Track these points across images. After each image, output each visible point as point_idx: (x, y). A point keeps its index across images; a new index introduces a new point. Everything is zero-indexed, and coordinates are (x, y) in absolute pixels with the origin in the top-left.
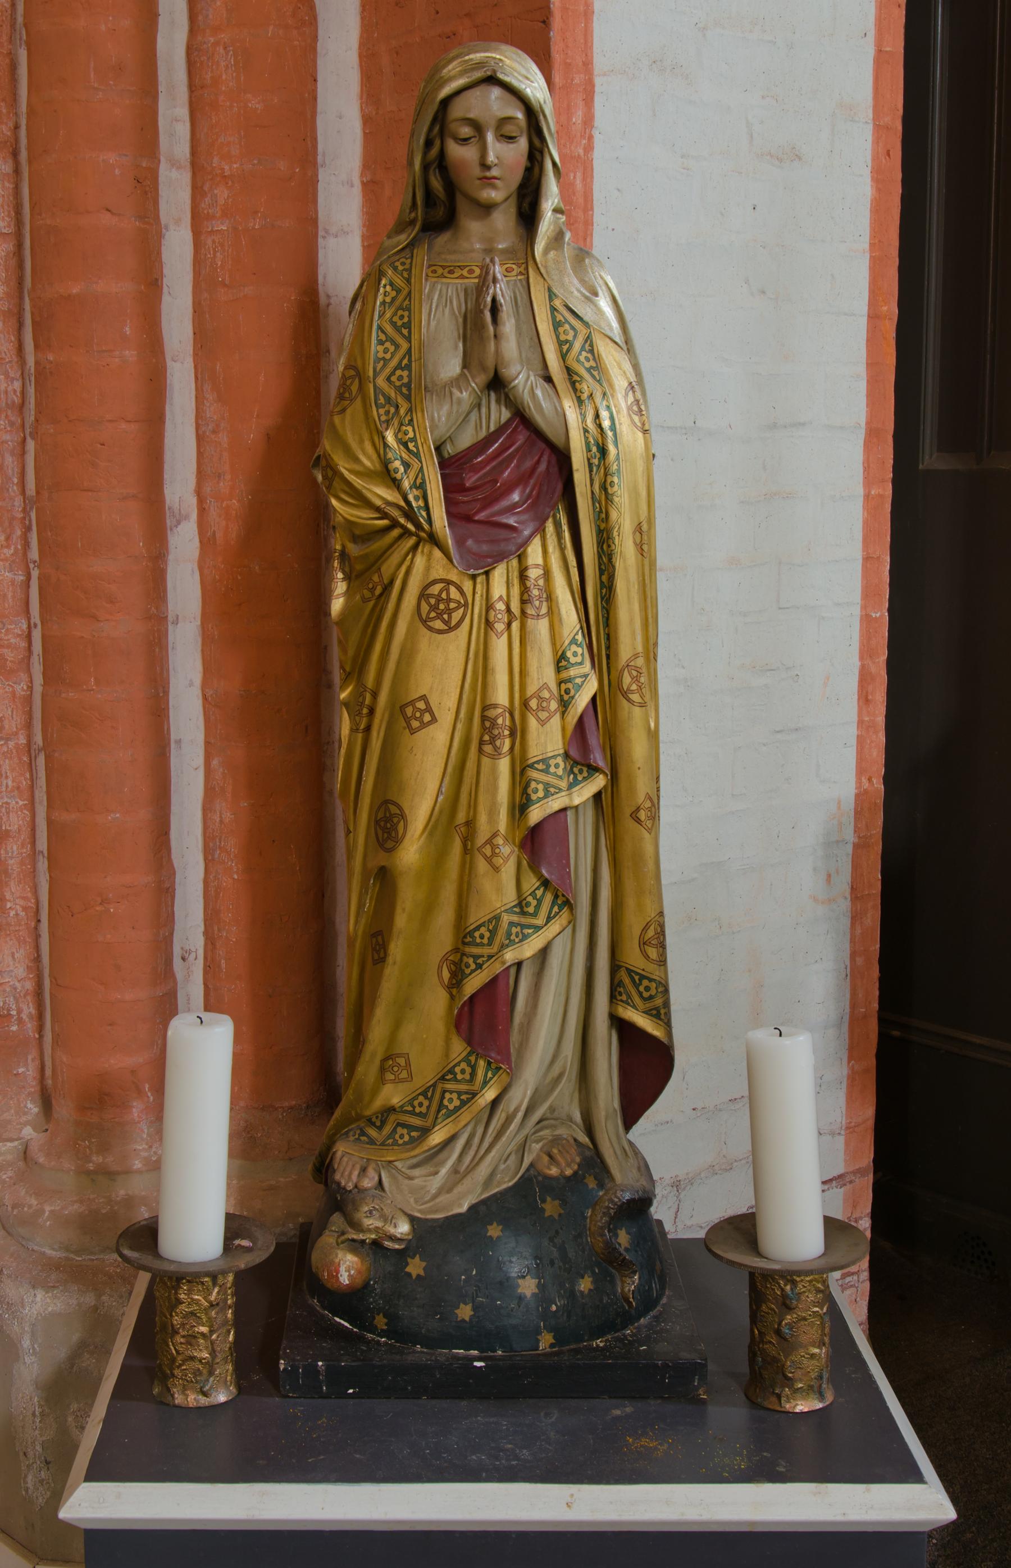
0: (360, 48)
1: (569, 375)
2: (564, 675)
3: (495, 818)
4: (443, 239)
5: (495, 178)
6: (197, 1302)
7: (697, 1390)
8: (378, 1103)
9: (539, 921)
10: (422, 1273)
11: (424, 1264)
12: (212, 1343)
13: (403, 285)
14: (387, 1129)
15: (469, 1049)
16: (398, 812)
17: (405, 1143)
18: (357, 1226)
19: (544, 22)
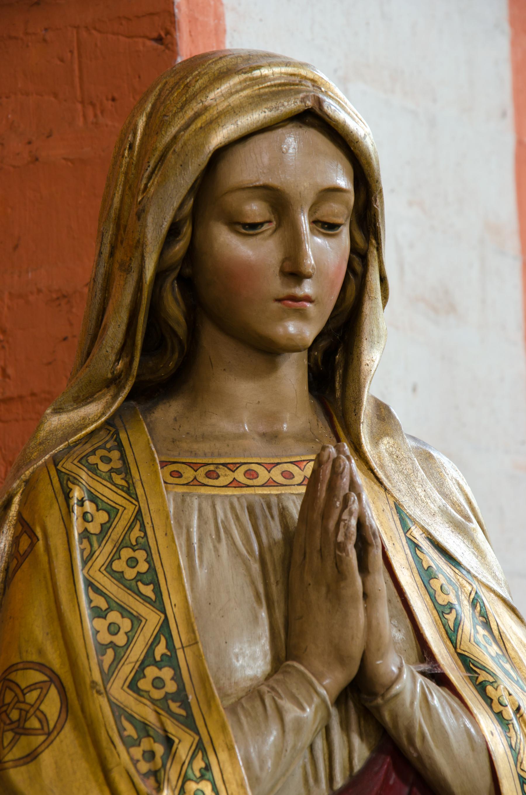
1: (468, 669)
4: (167, 413)
5: (308, 299)
13: (119, 500)
19: (159, 40)
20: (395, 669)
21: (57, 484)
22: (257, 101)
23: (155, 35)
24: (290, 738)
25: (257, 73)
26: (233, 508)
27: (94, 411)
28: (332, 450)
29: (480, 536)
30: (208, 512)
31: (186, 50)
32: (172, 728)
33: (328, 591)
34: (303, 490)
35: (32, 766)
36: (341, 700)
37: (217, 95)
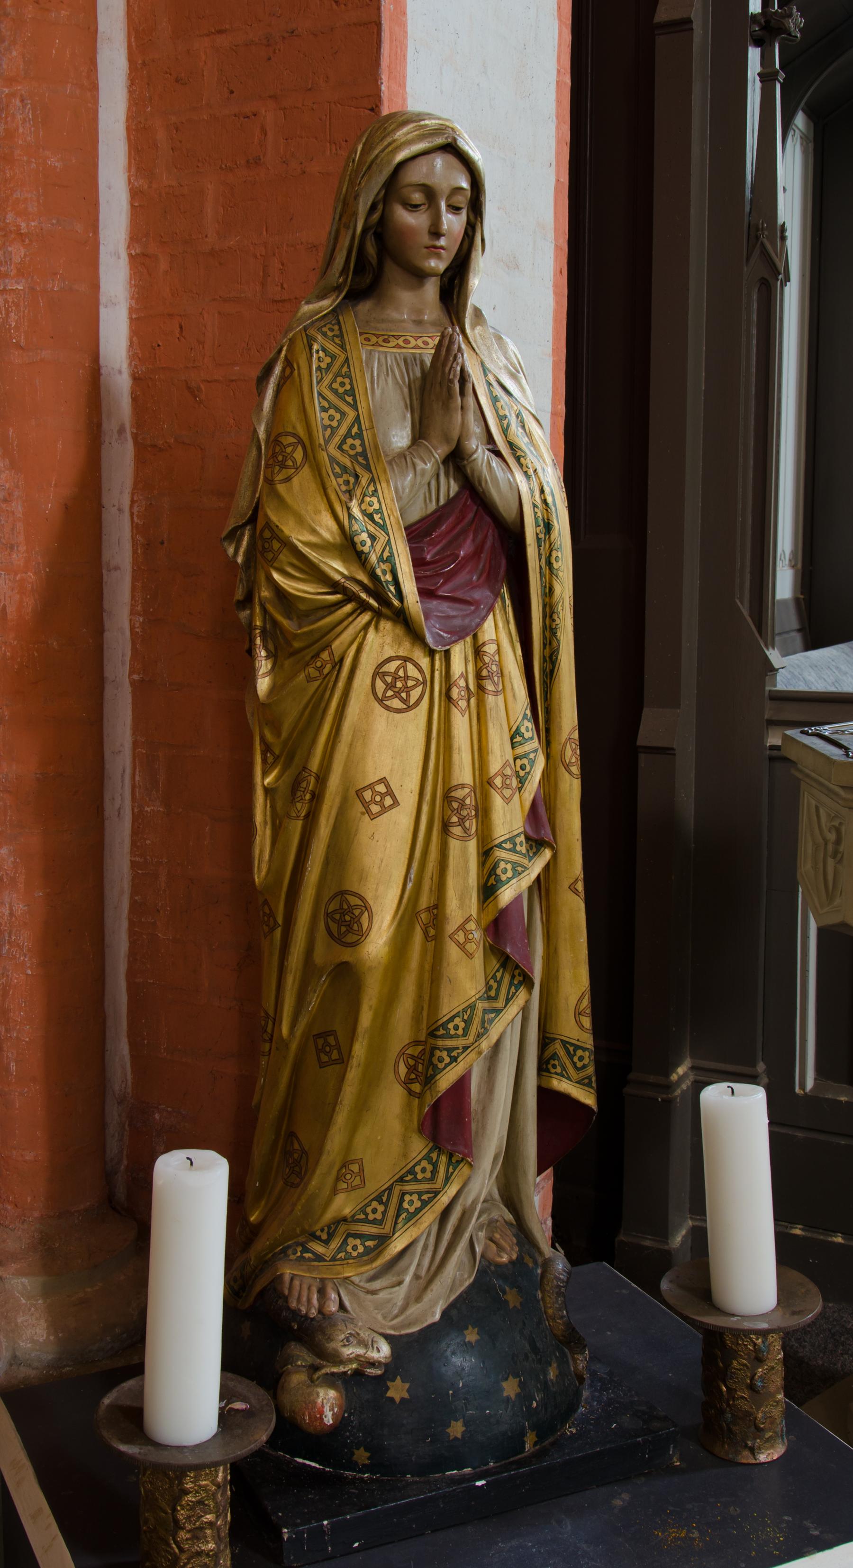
0: (127, 120)
1: (512, 449)
2: (520, 750)
3: (461, 904)
4: (365, 307)
5: (442, 248)
6: (205, 1488)
7: (672, 1459)
8: (329, 1215)
9: (500, 1004)
10: (406, 1396)
11: (407, 1385)
12: (219, 1529)
14: (335, 1244)
15: (431, 1144)
16: (360, 903)
17: (360, 1255)
18: (336, 1359)
19: (372, 110)
20: (474, 447)
21: (305, 341)
22: (421, 138)
23: (370, 107)
24: (419, 478)
25: (422, 123)
26: (395, 357)
27: (326, 304)
28: (450, 330)
29: (524, 381)
30: (383, 360)
31: (385, 111)
32: (359, 470)
33: (443, 404)
34: (433, 351)
35: (288, 484)
36: (446, 461)
37: (400, 134)
